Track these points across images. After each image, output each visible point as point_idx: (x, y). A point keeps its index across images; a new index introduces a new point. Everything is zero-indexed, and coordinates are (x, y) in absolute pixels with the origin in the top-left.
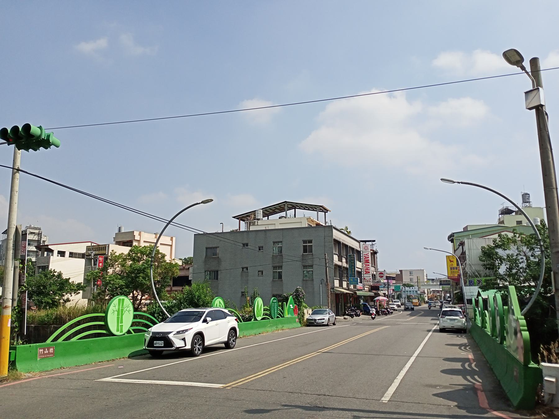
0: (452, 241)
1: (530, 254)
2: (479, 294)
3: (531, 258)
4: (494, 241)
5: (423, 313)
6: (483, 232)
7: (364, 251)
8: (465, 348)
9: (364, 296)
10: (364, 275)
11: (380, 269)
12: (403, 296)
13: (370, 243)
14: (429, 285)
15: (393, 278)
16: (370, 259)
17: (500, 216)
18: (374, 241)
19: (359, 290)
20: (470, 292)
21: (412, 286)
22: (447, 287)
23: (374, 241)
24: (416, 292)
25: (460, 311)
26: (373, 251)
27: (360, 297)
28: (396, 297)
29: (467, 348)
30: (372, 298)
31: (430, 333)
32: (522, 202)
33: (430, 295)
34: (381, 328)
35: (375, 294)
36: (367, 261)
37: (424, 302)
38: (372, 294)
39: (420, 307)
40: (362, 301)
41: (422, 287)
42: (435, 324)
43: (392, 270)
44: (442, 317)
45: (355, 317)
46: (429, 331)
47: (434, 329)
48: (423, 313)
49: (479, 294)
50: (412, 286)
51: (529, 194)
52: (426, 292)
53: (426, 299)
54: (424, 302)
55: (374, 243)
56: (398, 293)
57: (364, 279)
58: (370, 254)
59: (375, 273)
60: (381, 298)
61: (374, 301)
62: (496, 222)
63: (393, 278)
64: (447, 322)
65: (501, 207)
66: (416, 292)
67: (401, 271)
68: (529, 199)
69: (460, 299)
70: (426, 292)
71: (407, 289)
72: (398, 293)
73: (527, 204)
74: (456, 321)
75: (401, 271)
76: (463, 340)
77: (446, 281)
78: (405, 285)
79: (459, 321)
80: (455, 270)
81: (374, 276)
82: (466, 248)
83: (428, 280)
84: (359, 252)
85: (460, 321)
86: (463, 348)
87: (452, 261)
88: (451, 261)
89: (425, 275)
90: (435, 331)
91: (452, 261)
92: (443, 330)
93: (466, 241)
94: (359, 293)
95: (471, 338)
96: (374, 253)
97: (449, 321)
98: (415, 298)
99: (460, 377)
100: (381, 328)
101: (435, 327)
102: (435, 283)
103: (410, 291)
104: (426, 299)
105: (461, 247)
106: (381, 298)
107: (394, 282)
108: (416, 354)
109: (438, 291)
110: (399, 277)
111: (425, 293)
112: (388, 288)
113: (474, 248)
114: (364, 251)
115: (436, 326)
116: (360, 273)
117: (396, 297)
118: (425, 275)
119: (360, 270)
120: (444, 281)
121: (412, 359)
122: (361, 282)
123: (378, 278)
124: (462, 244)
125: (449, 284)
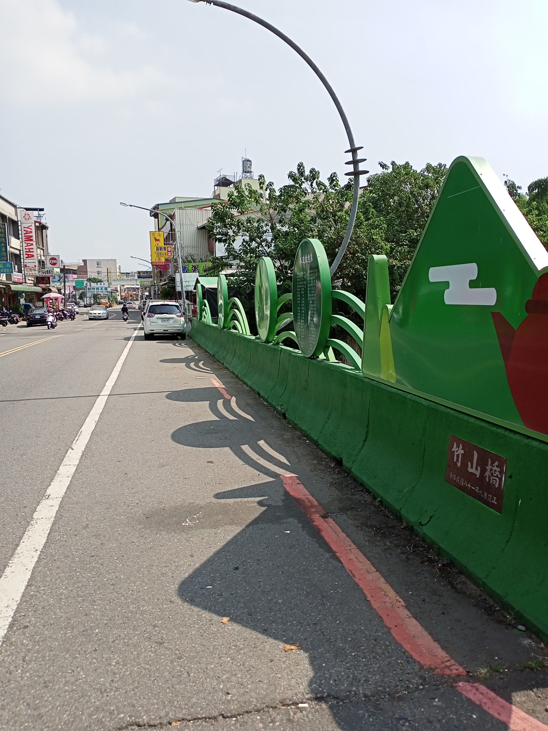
0: (156, 216)
1: (277, 218)
2: (198, 281)
3: (277, 225)
4: (230, 196)
5: (115, 315)
6: (198, 204)
7: (23, 220)
8: (197, 365)
9: (26, 292)
10: (25, 261)
11: (52, 252)
12: (89, 295)
13: (36, 213)
14: (123, 280)
15: (74, 272)
16: (33, 234)
17: (216, 187)
18: (42, 210)
19: (15, 283)
20: (187, 280)
21: (101, 281)
22: (147, 282)
23: (42, 210)
24: (106, 289)
25: (177, 306)
26: (40, 223)
27: (17, 294)
28: (77, 297)
29: (201, 364)
30: (39, 296)
31: (130, 343)
32: (241, 171)
33: (123, 294)
34: (45, 340)
35: (44, 289)
36: (29, 239)
37: (117, 302)
38: (38, 289)
39: (111, 308)
40: (22, 301)
41: (113, 283)
42: (135, 329)
43: (71, 260)
44: (149, 316)
45: (9, 325)
46: (128, 339)
47: (135, 335)
48: (115, 315)
49: (198, 281)
50: (101, 281)
51: (250, 161)
52: (119, 290)
53: (119, 298)
54: (117, 302)
55: (41, 213)
56: (81, 291)
57: (26, 266)
58: (33, 227)
59: (43, 258)
60: (52, 295)
61: (43, 300)
62: (210, 196)
63: (74, 272)
64: (155, 323)
65: (217, 176)
66: (106, 289)
67: (85, 261)
68: (250, 168)
69: (170, 292)
70: (119, 290)
71: (93, 285)
72: (81, 291)
73: (248, 174)
74: (171, 321)
75: (85, 261)
76: (184, 351)
77: (147, 272)
78: (90, 280)
79: (176, 321)
80: (163, 252)
81: (42, 263)
82: (176, 223)
83: (122, 273)
84: (14, 223)
85: (176, 321)
86: (192, 365)
87: (159, 240)
88: (157, 240)
89: (118, 267)
90: (138, 338)
91: (159, 240)
92: (150, 337)
93: (177, 212)
94: (13, 287)
95: (196, 346)
96: (42, 228)
97: (160, 321)
98: (105, 297)
99: (226, 453)
100: (45, 340)
101: (136, 333)
102: (130, 278)
103: (98, 289)
104: (119, 298)
105: (168, 223)
106: (52, 295)
107: (75, 276)
108: (107, 391)
109: (134, 289)
110: (82, 270)
111: (117, 291)
112: (65, 282)
113: (189, 223)
114: (23, 220)
115: (137, 331)
116: (17, 258)
117: (77, 297)
118: (118, 267)
119: (18, 252)
120: (144, 272)
121: (100, 403)
122: (20, 271)
123: (48, 265)
124: (172, 217)
125: (151, 277)
